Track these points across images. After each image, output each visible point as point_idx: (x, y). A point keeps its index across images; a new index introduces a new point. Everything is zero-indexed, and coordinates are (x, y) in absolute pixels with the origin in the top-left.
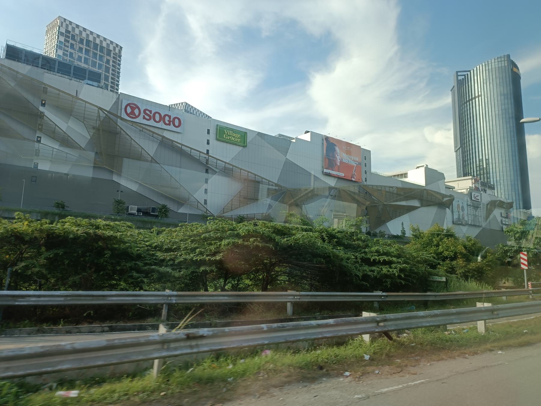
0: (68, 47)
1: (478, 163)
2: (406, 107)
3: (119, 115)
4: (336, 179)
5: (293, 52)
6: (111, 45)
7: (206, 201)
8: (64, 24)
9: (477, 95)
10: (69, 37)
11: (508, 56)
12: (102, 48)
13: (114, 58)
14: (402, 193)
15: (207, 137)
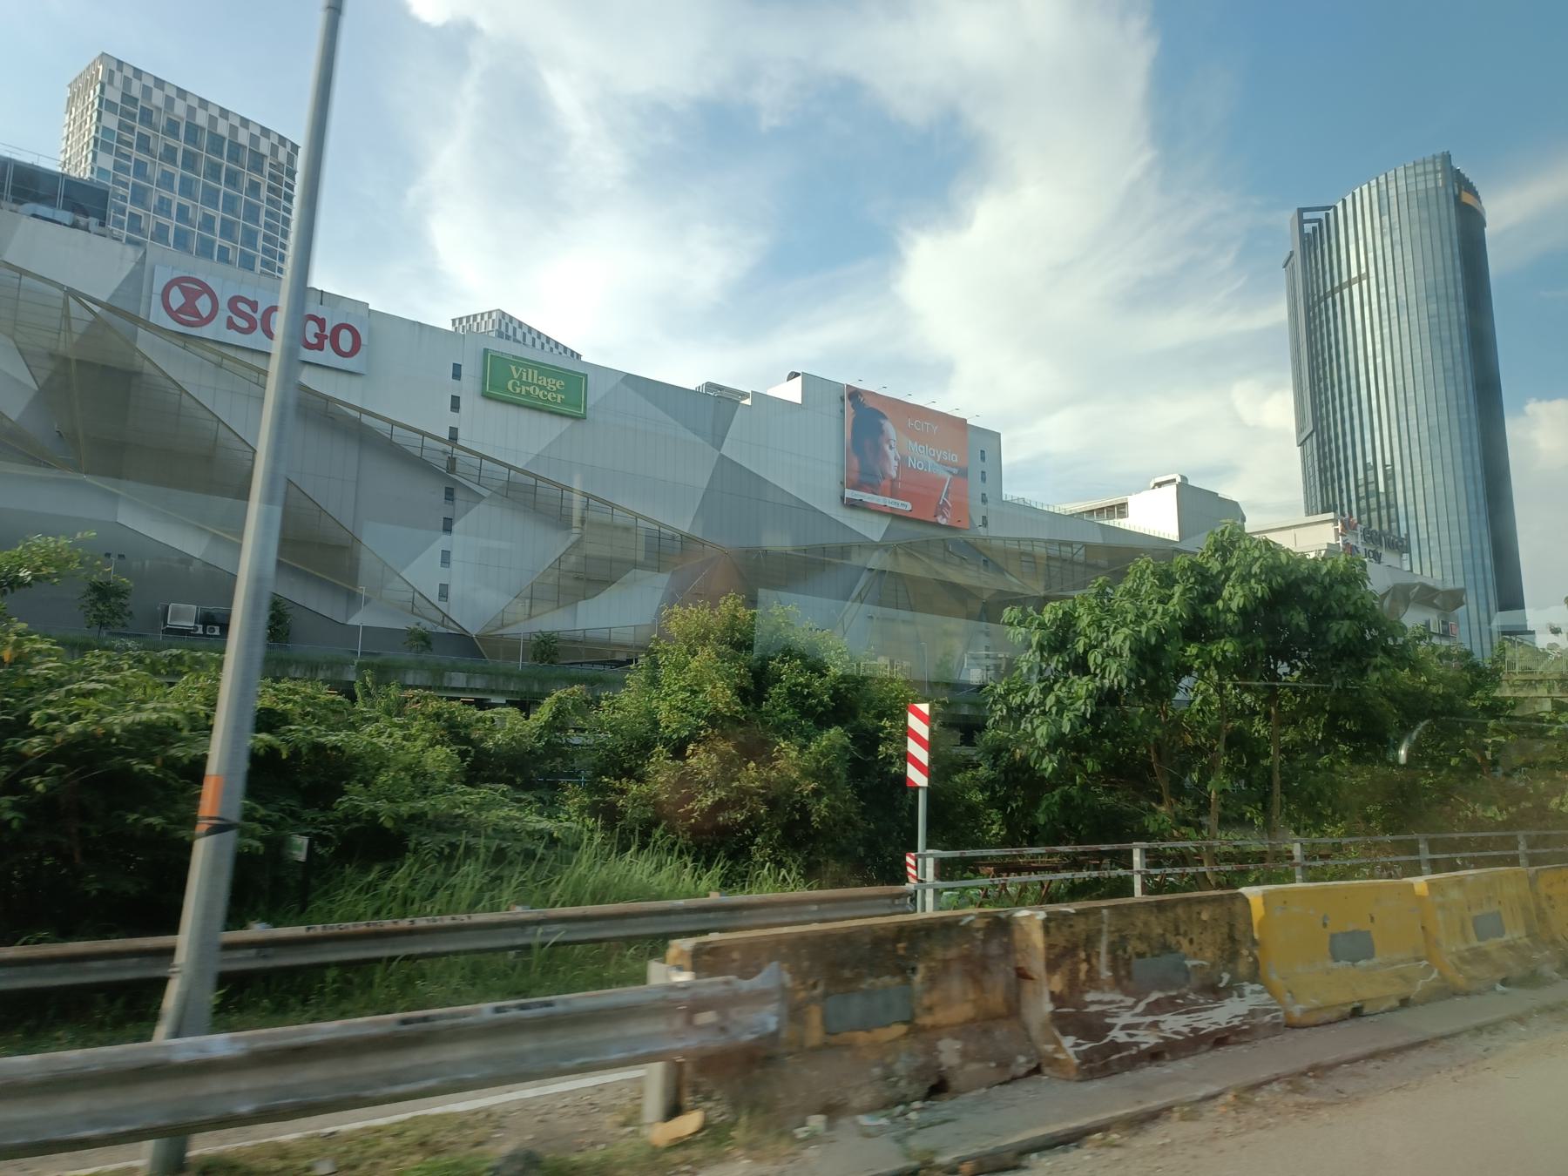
0: (130, 145)
1: (1361, 475)
2: (1180, 326)
3: (142, 316)
4: (886, 522)
5: (850, 171)
6: (263, 140)
7: (444, 592)
8: (118, 77)
9: (1354, 274)
10: (133, 117)
11: (1447, 158)
12: (236, 148)
13: (272, 176)
14: (1103, 562)
15: (453, 387)
